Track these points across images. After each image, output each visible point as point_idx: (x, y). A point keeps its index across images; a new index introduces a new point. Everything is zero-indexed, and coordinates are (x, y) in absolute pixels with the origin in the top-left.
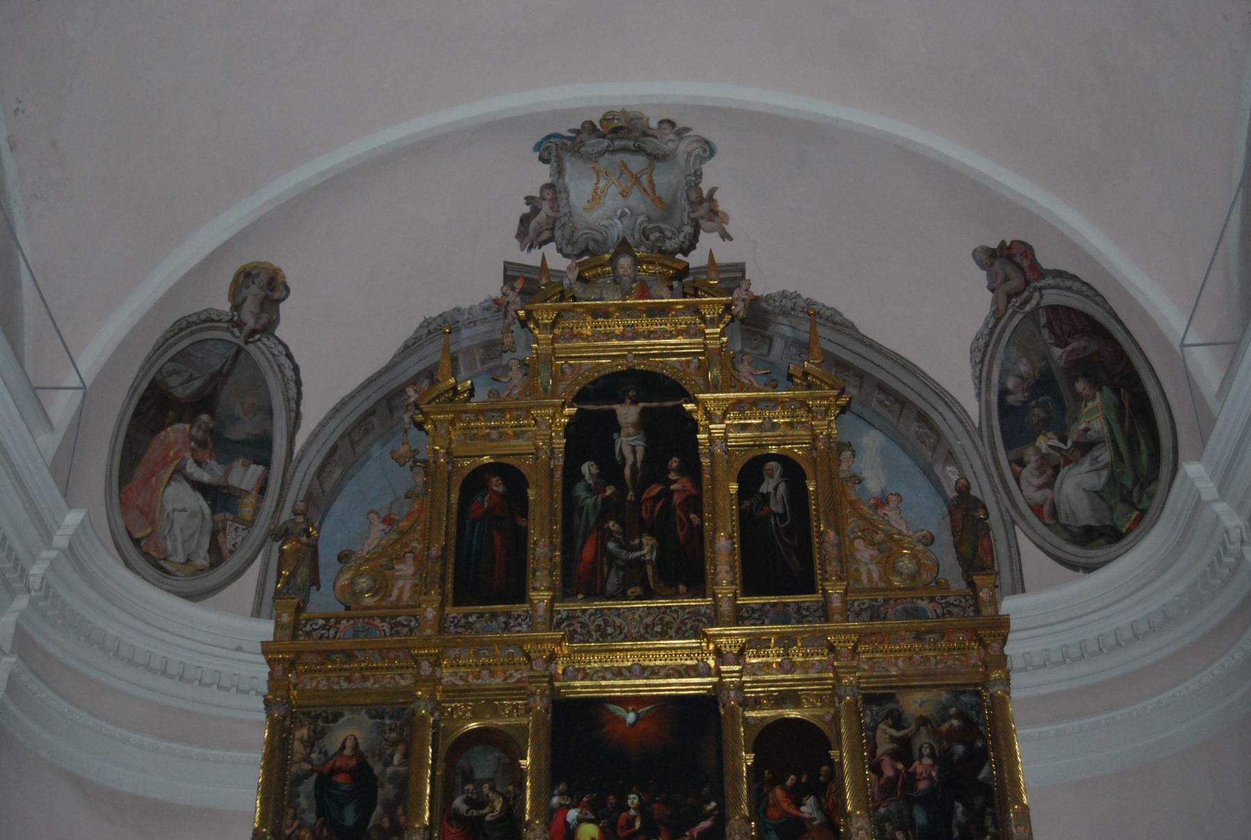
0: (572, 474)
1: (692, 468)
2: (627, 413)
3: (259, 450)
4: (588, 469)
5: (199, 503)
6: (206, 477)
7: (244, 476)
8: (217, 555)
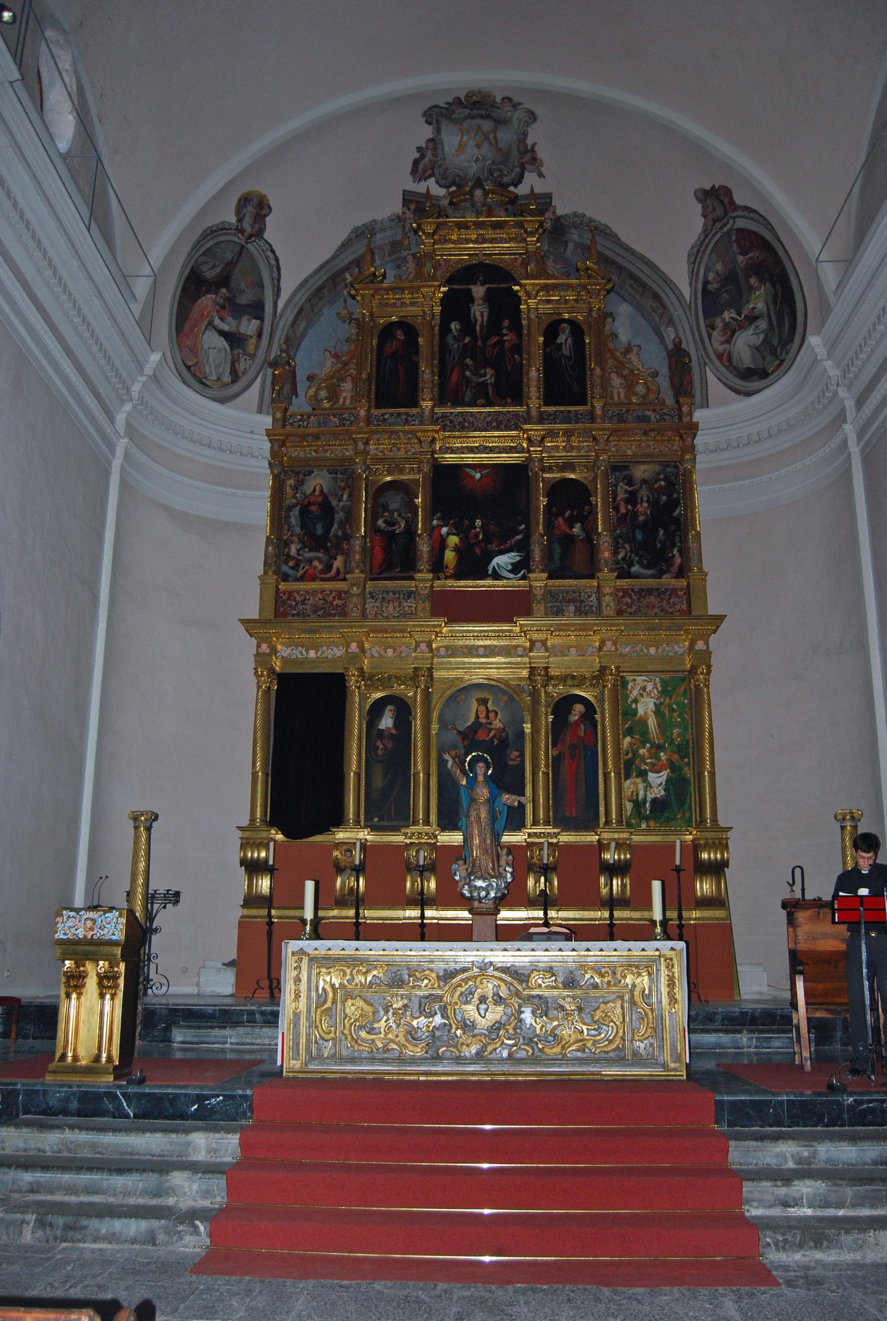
0: (445, 329)
1: (516, 327)
2: (478, 291)
3: (256, 310)
4: (455, 326)
5: (222, 343)
6: (226, 328)
7: (249, 327)
8: (235, 376)
